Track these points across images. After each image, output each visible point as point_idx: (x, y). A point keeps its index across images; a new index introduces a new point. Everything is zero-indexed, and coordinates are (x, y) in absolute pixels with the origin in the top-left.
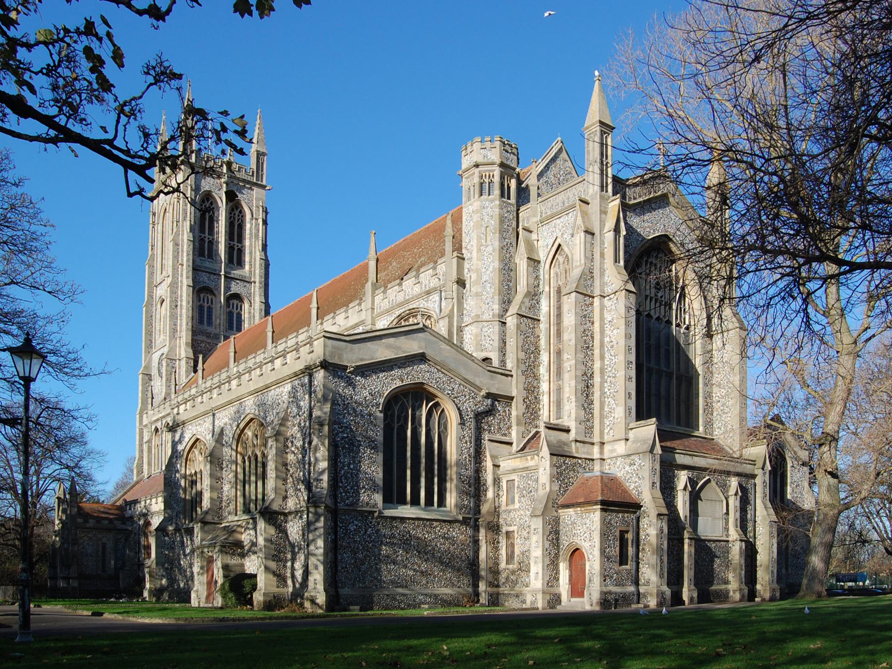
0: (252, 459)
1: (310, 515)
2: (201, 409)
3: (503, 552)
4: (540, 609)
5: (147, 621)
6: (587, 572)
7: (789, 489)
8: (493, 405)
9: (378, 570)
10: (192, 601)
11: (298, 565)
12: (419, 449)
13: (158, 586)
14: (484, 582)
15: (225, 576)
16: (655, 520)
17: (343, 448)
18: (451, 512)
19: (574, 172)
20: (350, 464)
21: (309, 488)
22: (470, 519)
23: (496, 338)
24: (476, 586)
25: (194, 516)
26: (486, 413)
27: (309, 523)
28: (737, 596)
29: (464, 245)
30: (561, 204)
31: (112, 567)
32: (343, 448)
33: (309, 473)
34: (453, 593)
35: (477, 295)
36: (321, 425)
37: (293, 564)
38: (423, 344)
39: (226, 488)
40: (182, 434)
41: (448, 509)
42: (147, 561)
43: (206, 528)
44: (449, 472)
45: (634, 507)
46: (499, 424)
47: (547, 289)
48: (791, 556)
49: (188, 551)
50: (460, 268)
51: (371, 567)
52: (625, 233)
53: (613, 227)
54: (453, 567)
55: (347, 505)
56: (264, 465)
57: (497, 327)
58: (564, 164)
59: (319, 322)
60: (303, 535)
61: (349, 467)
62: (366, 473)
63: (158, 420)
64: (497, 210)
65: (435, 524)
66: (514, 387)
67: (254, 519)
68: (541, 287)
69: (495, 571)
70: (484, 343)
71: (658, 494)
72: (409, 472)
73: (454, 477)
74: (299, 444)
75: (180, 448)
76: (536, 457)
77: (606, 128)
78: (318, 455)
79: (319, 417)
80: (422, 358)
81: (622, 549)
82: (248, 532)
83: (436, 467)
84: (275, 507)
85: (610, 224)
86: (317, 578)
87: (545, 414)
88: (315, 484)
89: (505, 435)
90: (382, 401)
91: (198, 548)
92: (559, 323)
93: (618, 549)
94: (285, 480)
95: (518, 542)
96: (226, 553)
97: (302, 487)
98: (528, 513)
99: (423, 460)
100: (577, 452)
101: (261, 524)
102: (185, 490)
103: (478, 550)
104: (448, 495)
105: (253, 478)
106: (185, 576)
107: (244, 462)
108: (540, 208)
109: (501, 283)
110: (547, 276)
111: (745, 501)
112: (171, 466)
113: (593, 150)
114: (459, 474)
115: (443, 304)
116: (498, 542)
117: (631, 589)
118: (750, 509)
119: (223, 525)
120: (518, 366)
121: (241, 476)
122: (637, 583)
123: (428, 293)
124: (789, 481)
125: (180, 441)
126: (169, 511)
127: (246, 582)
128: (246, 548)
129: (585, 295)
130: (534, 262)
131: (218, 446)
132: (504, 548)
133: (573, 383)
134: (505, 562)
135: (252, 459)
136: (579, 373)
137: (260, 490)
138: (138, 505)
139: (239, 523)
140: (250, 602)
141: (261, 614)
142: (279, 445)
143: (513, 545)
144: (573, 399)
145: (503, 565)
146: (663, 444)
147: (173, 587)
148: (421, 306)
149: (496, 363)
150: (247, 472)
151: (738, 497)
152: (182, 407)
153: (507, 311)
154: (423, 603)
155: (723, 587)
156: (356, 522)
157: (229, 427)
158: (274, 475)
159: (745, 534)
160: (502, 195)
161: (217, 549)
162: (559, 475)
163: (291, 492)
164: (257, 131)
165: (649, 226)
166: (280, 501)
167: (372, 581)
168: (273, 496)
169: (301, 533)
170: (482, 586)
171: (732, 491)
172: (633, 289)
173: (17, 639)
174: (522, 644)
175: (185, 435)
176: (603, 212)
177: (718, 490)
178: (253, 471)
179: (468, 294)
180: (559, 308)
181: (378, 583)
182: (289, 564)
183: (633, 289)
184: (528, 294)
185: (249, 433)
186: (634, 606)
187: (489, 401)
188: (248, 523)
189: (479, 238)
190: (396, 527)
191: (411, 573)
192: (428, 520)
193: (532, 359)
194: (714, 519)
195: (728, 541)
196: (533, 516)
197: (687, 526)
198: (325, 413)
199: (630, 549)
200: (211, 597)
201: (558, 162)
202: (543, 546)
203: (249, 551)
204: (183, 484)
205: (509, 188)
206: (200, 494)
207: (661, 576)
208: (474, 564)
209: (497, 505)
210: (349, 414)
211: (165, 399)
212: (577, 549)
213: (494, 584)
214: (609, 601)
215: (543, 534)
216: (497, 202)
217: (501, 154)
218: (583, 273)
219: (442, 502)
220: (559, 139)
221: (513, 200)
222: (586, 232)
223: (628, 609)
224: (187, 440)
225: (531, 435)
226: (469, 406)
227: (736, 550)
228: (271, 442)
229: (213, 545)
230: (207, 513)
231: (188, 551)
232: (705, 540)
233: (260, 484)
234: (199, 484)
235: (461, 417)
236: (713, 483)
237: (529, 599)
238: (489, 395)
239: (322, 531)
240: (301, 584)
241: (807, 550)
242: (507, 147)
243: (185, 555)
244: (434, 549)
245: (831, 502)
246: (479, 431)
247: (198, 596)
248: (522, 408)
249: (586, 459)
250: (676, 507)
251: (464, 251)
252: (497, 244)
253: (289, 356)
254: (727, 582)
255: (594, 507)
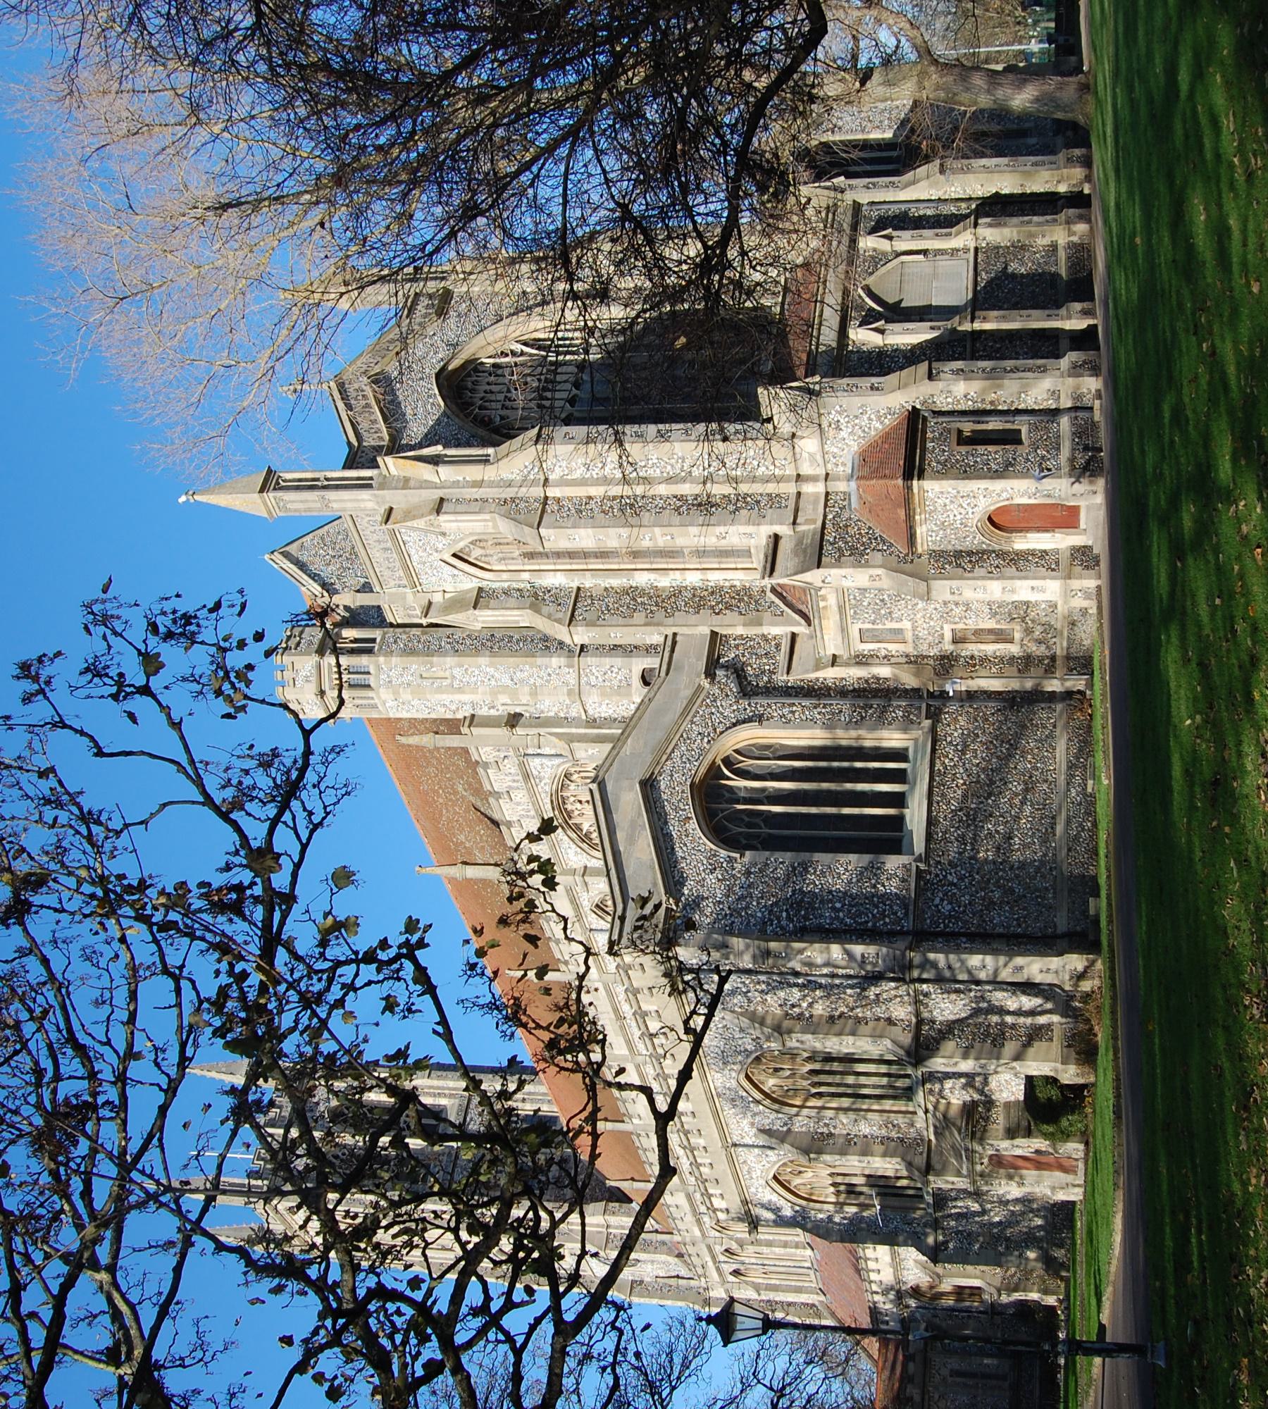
0: (816, 1079)
1: (925, 976)
2: (723, 1167)
3: (990, 649)
4: (1099, 582)
5: (1118, 1238)
6: (1032, 501)
7: (875, 135)
8: (726, 667)
9: (1023, 865)
10: (1072, 1198)
11: (1012, 1003)
12: (805, 792)
13: (1039, 1265)
14: (1045, 682)
15: (1028, 1134)
16: (940, 385)
17: (808, 919)
18: (916, 740)
19: (320, 532)
20: (834, 908)
21: (875, 978)
22: (929, 706)
23: (607, 661)
24: (1052, 697)
25: (911, 1192)
26: (742, 679)
27: (939, 980)
28: (1081, 228)
29: (449, 716)
30: (388, 554)
31: (996, 1362)
32: (806, 918)
33: (849, 977)
34: (1065, 737)
35: (534, 693)
36: (768, 953)
37: (1009, 1013)
38: (626, 783)
39: (864, 1128)
40: (763, 1206)
41: (910, 744)
42: (986, 1297)
43: (938, 1167)
44: (844, 743)
45: (914, 419)
46: (759, 657)
47: (526, 576)
48: (1005, 136)
49: (975, 1207)
50: (489, 722)
51: (1017, 876)
52: (440, 447)
53: (431, 467)
54: (1018, 736)
55: (906, 914)
56: (829, 1058)
57: (588, 660)
58: (309, 550)
59: (563, 967)
60: (957, 991)
61: (839, 910)
62: (850, 882)
63: (718, 1269)
64: (395, 660)
65: (938, 766)
66: (695, 630)
67: (930, 1077)
68: (522, 586)
69: (1026, 663)
70: (615, 682)
71: (893, 378)
72: (846, 811)
73: (853, 733)
74: (796, 994)
75: (787, 1212)
76: (822, 592)
77: (270, 482)
78: (819, 961)
79: (754, 957)
80: (649, 786)
81: (989, 440)
82: (947, 1092)
83: (835, 764)
84: (907, 1039)
85: (426, 472)
86: (1036, 968)
87: (746, 576)
88: (869, 968)
89: (778, 646)
90: (723, 853)
91: (974, 1182)
92: (585, 555)
93: (991, 448)
94: (858, 1021)
95: (972, 623)
96: (985, 1131)
97: (872, 992)
98: (921, 605)
99: (825, 786)
100: (814, 521)
101: (938, 1064)
102: (864, 1207)
103: (985, 692)
104: (886, 744)
105: (850, 1080)
106: (1023, 1213)
107: (820, 1095)
108: (391, 588)
109: (514, 653)
110: (505, 576)
111: (903, 221)
112: (822, 1230)
113: (298, 502)
114: (848, 725)
115: (547, 751)
116: (972, 657)
117: (1065, 421)
118: (915, 211)
119: (932, 1137)
120: (658, 624)
121: (846, 1102)
122: (1054, 413)
123: (527, 776)
124: (860, 136)
125: (776, 1210)
126: (901, 1238)
127: (1042, 1094)
128: (976, 1097)
129: (543, 511)
130: (480, 598)
131: (790, 1139)
132: (983, 647)
133: (694, 530)
134: (1008, 646)
135: (816, 1079)
136: (677, 519)
137: (872, 1068)
138: (881, 1305)
139: (930, 1107)
140: (1078, 1090)
141: (1105, 1058)
142: (798, 1028)
143: (977, 632)
144: (722, 529)
145: (1014, 649)
146: (800, 372)
147: (1041, 1239)
148: (547, 788)
149: (652, 662)
150: (841, 1090)
151: (895, 233)
152: (718, 1203)
153: (561, 643)
154: (1085, 789)
155: (1062, 254)
156: (937, 901)
157: (757, 1118)
158: (851, 1039)
159: (967, 216)
160: (369, 651)
161: (978, 1148)
162: (856, 552)
163: (879, 1011)
164: (213, 1074)
165: (424, 406)
166: (896, 1031)
167: (1043, 876)
168: (888, 1043)
169: (953, 996)
170: (1053, 685)
171: (885, 245)
172: (536, 430)
173: (1161, 1363)
174: (1184, 613)
175: (765, 1200)
176: (405, 483)
177: (883, 270)
178: (837, 1079)
179: (532, 710)
180: (558, 555)
181: (1045, 867)
182: (1009, 1019)
183: (536, 430)
184: (535, 608)
185: (770, 1083)
186: (1097, 416)
187: (720, 673)
188: (931, 1091)
189: (440, 690)
190: (945, 833)
191: (1028, 809)
192: (932, 779)
193: (645, 600)
194: (935, 276)
195: (976, 249)
196: (927, 597)
197: (949, 325)
198: (747, 947)
199: (990, 426)
200: (1066, 1163)
201: (304, 558)
202: (983, 578)
203: (981, 1092)
204: (854, 1209)
205: (356, 641)
206: (875, 1181)
207: (1043, 370)
208: (1011, 701)
209: (904, 660)
210: (747, 907)
211: (680, 1256)
212: (990, 519)
213: (1050, 665)
214: (1088, 463)
215: (961, 578)
216: (382, 659)
217: (301, 654)
218: (507, 516)
219: (900, 755)
220: (267, 557)
221: (377, 634)
222: (438, 512)
223: (1102, 425)
224: (774, 1198)
225: (777, 601)
226: (730, 707)
227: (992, 234)
228: (792, 1043)
229: (970, 1154)
230: (909, 1165)
231: (975, 1207)
232: (975, 291)
233: (861, 1068)
234: (854, 1181)
235: (749, 720)
236: (870, 281)
237: (1079, 602)
238: (710, 674)
239: (951, 956)
240: (1047, 999)
241: (1000, 114)
242: (292, 643)
243: (984, 1212)
244: (984, 770)
245: (915, 79)
246: (772, 691)
247: (1062, 1188)
248: (731, 616)
249: (826, 506)
250: (914, 347)
251: (460, 716)
252: (450, 661)
253: (645, 1007)
254: (1054, 247)
255: (915, 490)
